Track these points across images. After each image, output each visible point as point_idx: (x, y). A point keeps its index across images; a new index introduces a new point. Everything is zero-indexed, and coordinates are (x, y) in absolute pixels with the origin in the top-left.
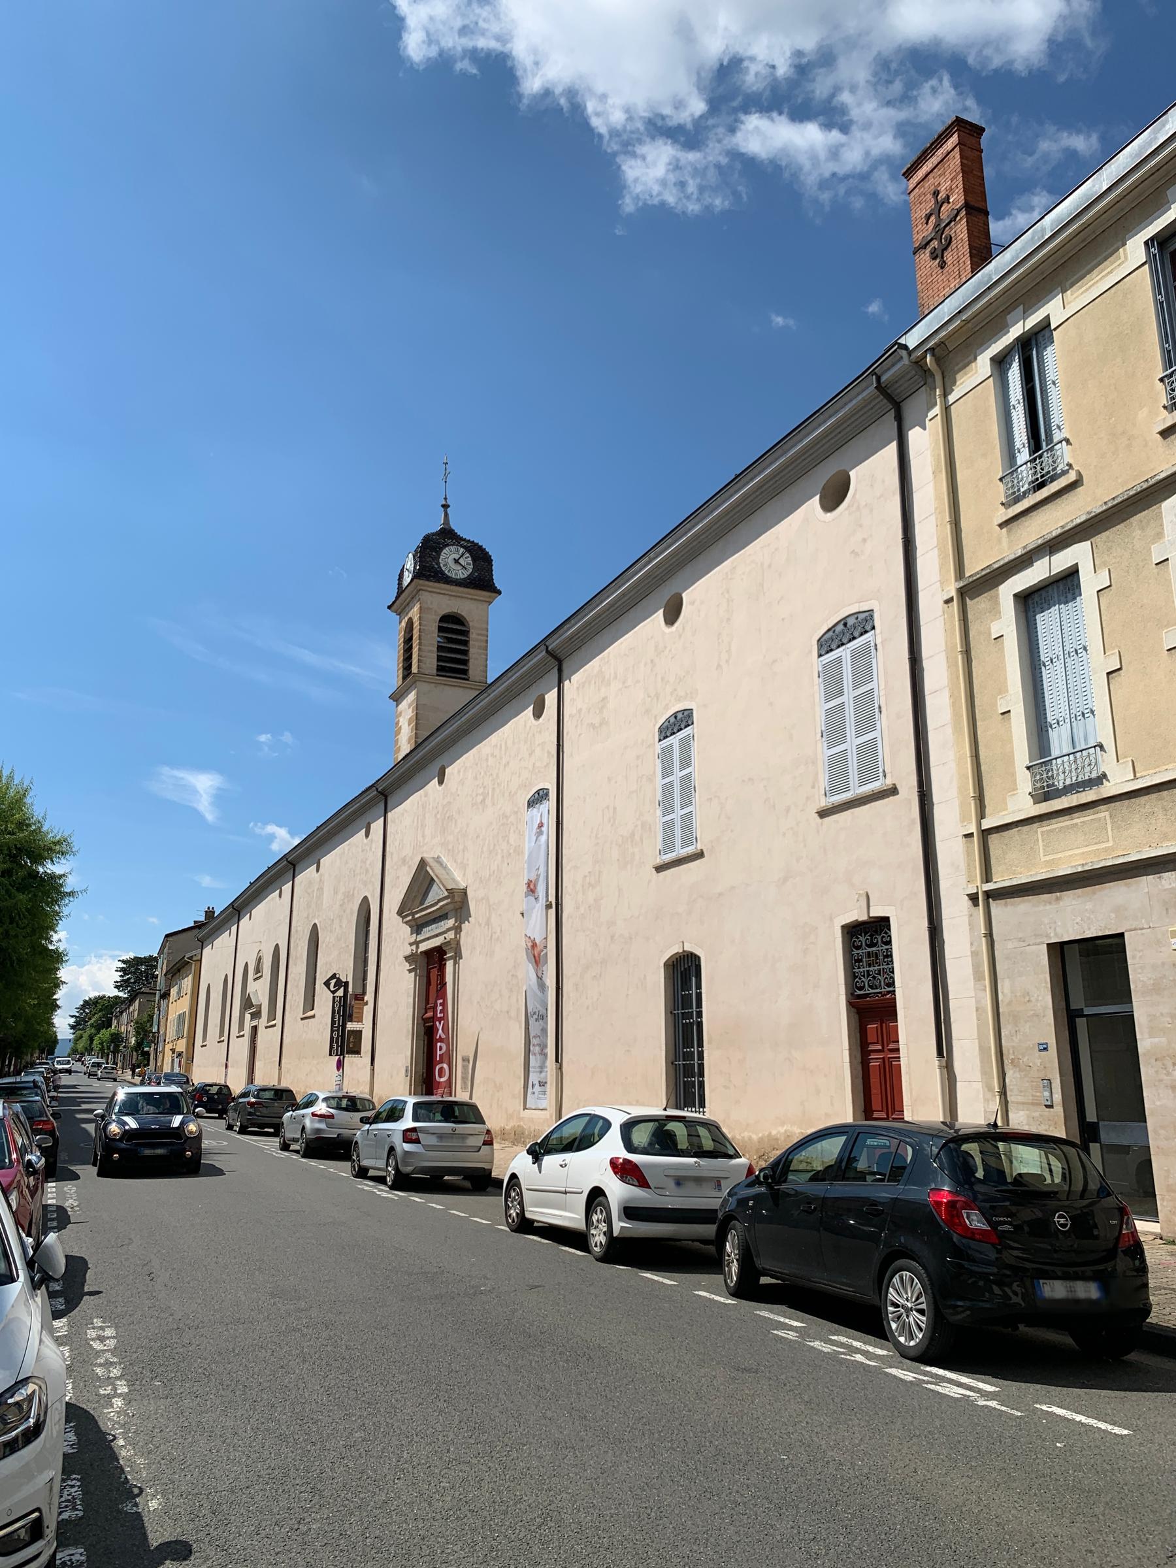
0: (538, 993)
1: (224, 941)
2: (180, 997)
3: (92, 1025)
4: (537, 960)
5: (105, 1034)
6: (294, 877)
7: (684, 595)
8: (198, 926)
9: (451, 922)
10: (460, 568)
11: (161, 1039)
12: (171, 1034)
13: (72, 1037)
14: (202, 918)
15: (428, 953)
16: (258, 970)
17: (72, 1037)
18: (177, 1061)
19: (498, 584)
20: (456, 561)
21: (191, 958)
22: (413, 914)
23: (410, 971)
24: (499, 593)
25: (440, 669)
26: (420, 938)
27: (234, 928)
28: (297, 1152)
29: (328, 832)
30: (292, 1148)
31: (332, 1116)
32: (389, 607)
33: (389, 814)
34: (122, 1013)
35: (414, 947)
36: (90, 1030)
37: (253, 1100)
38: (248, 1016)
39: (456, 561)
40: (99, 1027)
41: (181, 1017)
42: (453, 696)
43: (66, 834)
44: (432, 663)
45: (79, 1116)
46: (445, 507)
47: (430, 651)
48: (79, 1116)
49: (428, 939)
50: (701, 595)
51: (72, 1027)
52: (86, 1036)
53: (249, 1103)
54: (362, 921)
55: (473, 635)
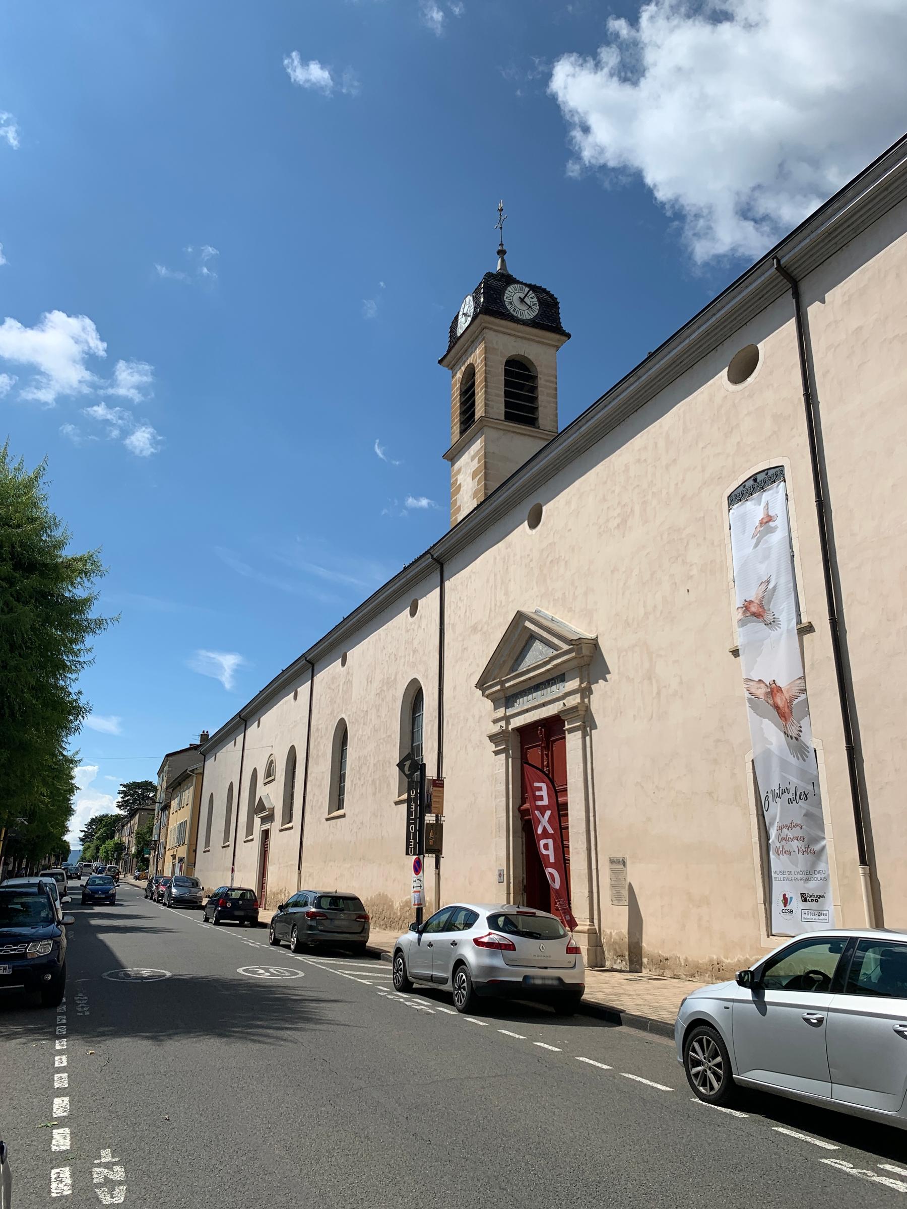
0: (792, 760)
1: (229, 753)
2: (180, 807)
3: (98, 838)
4: (783, 707)
5: (110, 844)
6: (313, 677)
7: (544, 508)
8: (193, 748)
10: (524, 307)
11: (162, 846)
12: (172, 839)
13: (81, 848)
15: (525, 732)
16: (270, 773)
17: (81, 848)
18: (178, 866)
19: (565, 326)
20: (522, 300)
21: (192, 771)
22: (502, 683)
23: (497, 753)
24: (568, 336)
25: (509, 417)
26: (510, 712)
29: (358, 621)
30: (282, 943)
31: (511, 947)
32: (440, 362)
34: (123, 826)
35: (503, 723)
36: (96, 842)
37: (314, 910)
38: (257, 821)
39: (522, 300)
40: (103, 839)
41: (182, 825)
42: (521, 445)
43: (82, 702)
44: (499, 409)
45: (94, 922)
46: (502, 253)
48: (94, 922)
49: (527, 711)
50: (355, 654)
51: (82, 840)
52: (93, 846)
53: (308, 913)
54: (339, 741)
55: (541, 382)
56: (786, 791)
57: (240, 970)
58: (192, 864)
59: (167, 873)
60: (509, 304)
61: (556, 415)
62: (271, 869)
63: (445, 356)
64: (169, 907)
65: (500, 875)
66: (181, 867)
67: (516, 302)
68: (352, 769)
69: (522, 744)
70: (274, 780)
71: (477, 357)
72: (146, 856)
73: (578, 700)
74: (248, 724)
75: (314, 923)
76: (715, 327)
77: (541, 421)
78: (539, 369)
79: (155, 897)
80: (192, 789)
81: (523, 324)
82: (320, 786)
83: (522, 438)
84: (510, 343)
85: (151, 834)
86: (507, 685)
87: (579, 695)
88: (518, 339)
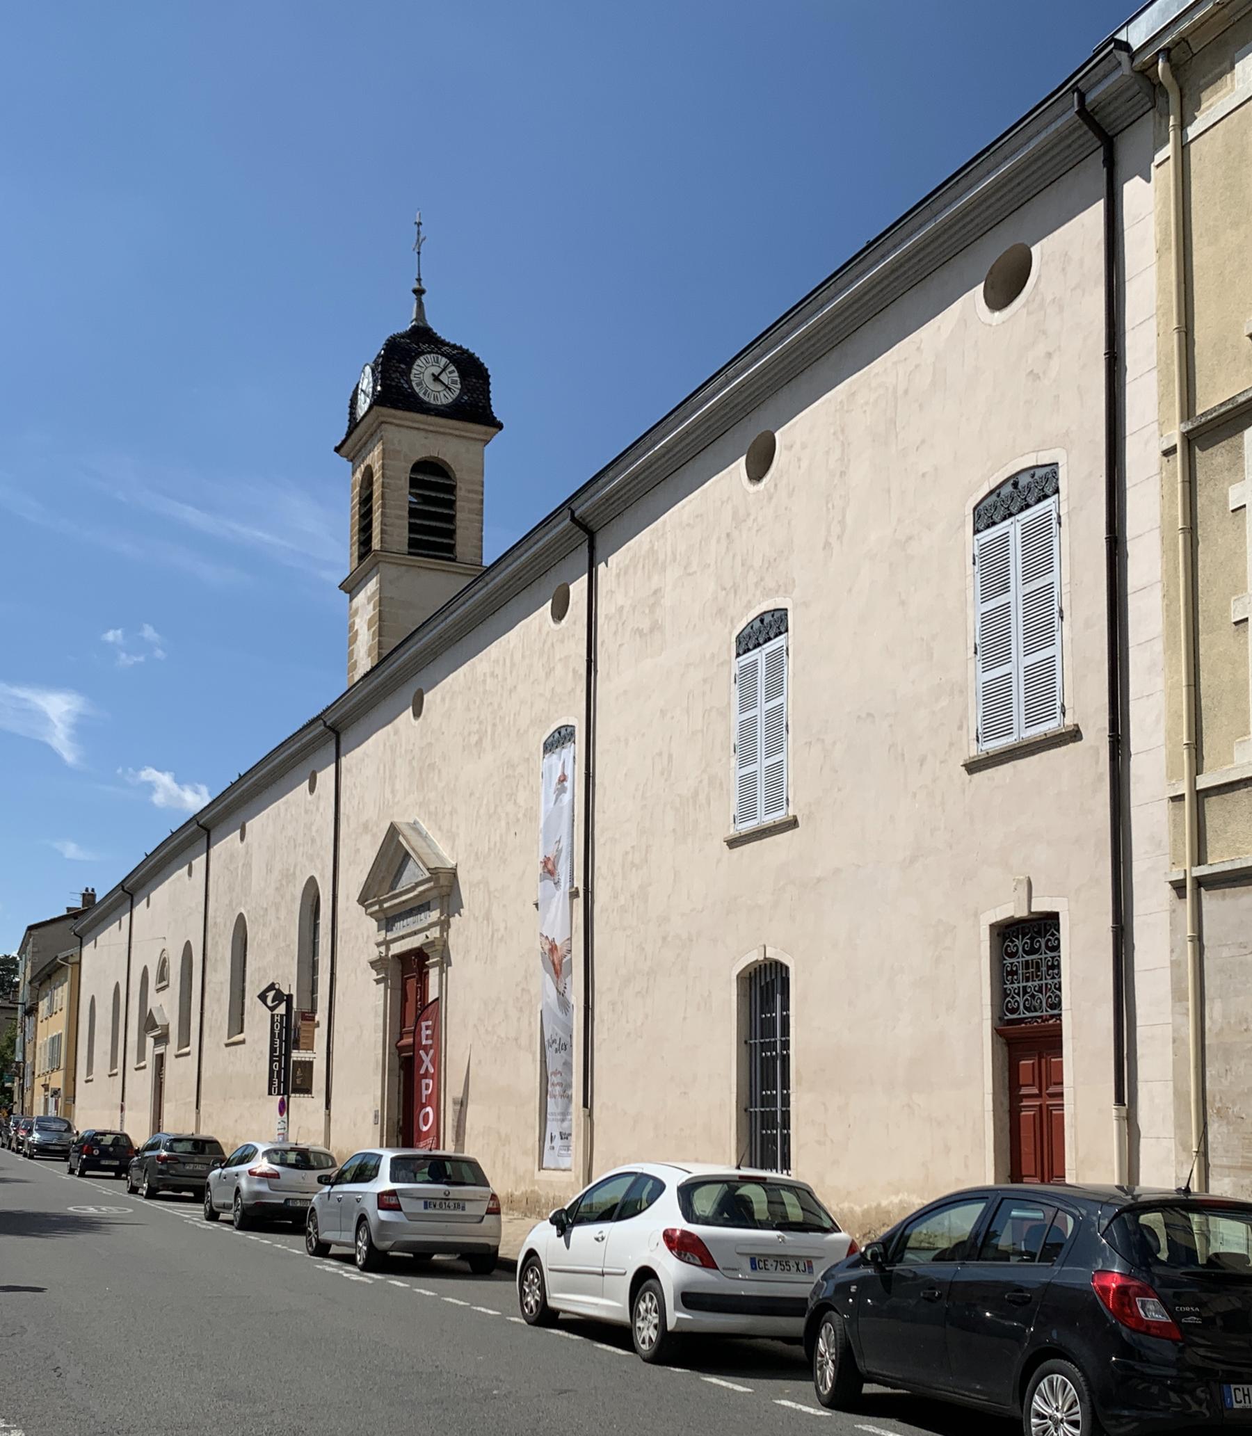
0: (559, 1014)
1: (111, 938)
2: (52, 1013)
4: (558, 969)
8: (73, 915)
9: (434, 915)
10: (440, 388)
11: (28, 1071)
12: (41, 1062)
14: (78, 904)
15: (403, 957)
16: (162, 976)
18: (52, 1101)
19: (498, 409)
20: (436, 378)
22: (381, 903)
23: (378, 982)
25: (415, 546)
26: (390, 936)
27: (326, 777)
28: (230, 1222)
29: (254, 784)
30: (222, 1216)
32: (337, 449)
33: (343, 760)
35: (383, 949)
38: (150, 1041)
41: (55, 1040)
42: (433, 585)
44: (401, 536)
47: (399, 517)
49: (403, 937)
53: (158, 1157)
55: (461, 493)
56: (554, 1041)
57: (71, 1209)
58: (71, 1098)
59: (38, 1111)
60: (418, 385)
61: (481, 540)
62: (167, 1107)
63: (344, 442)
64: (31, 1157)
65: (376, 1116)
66: (56, 1102)
67: (428, 380)
68: (252, 982)
69: (403, 974)
70: (167, 986)
71: (374, 458)
72: (8, 1085)
73: (438, 935)
74: (135, 899)
75: (164, 1167)
76: (536, 557)
77: (459, 549)
78: (458, 475)
79: (14, 1145)
80: (66, 985)
81: (436, 415)
82: (219, 1000)
83: (432, 573)
84: (415, 440)
85: (13, 1052)
86: (386, 905)
87: (438, 928)
88: (431, 435)
